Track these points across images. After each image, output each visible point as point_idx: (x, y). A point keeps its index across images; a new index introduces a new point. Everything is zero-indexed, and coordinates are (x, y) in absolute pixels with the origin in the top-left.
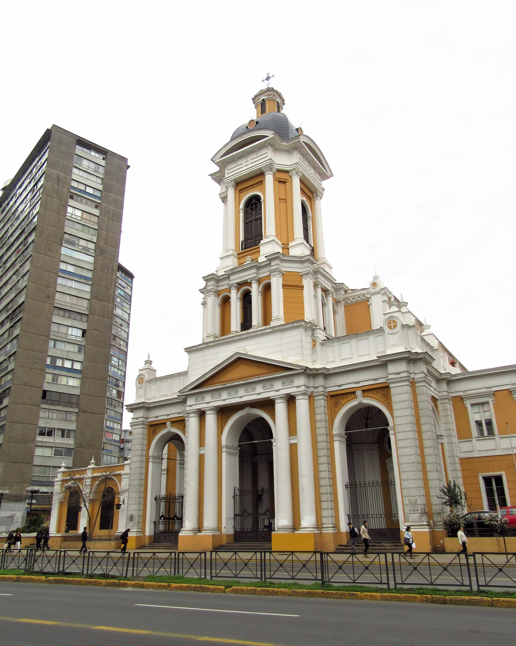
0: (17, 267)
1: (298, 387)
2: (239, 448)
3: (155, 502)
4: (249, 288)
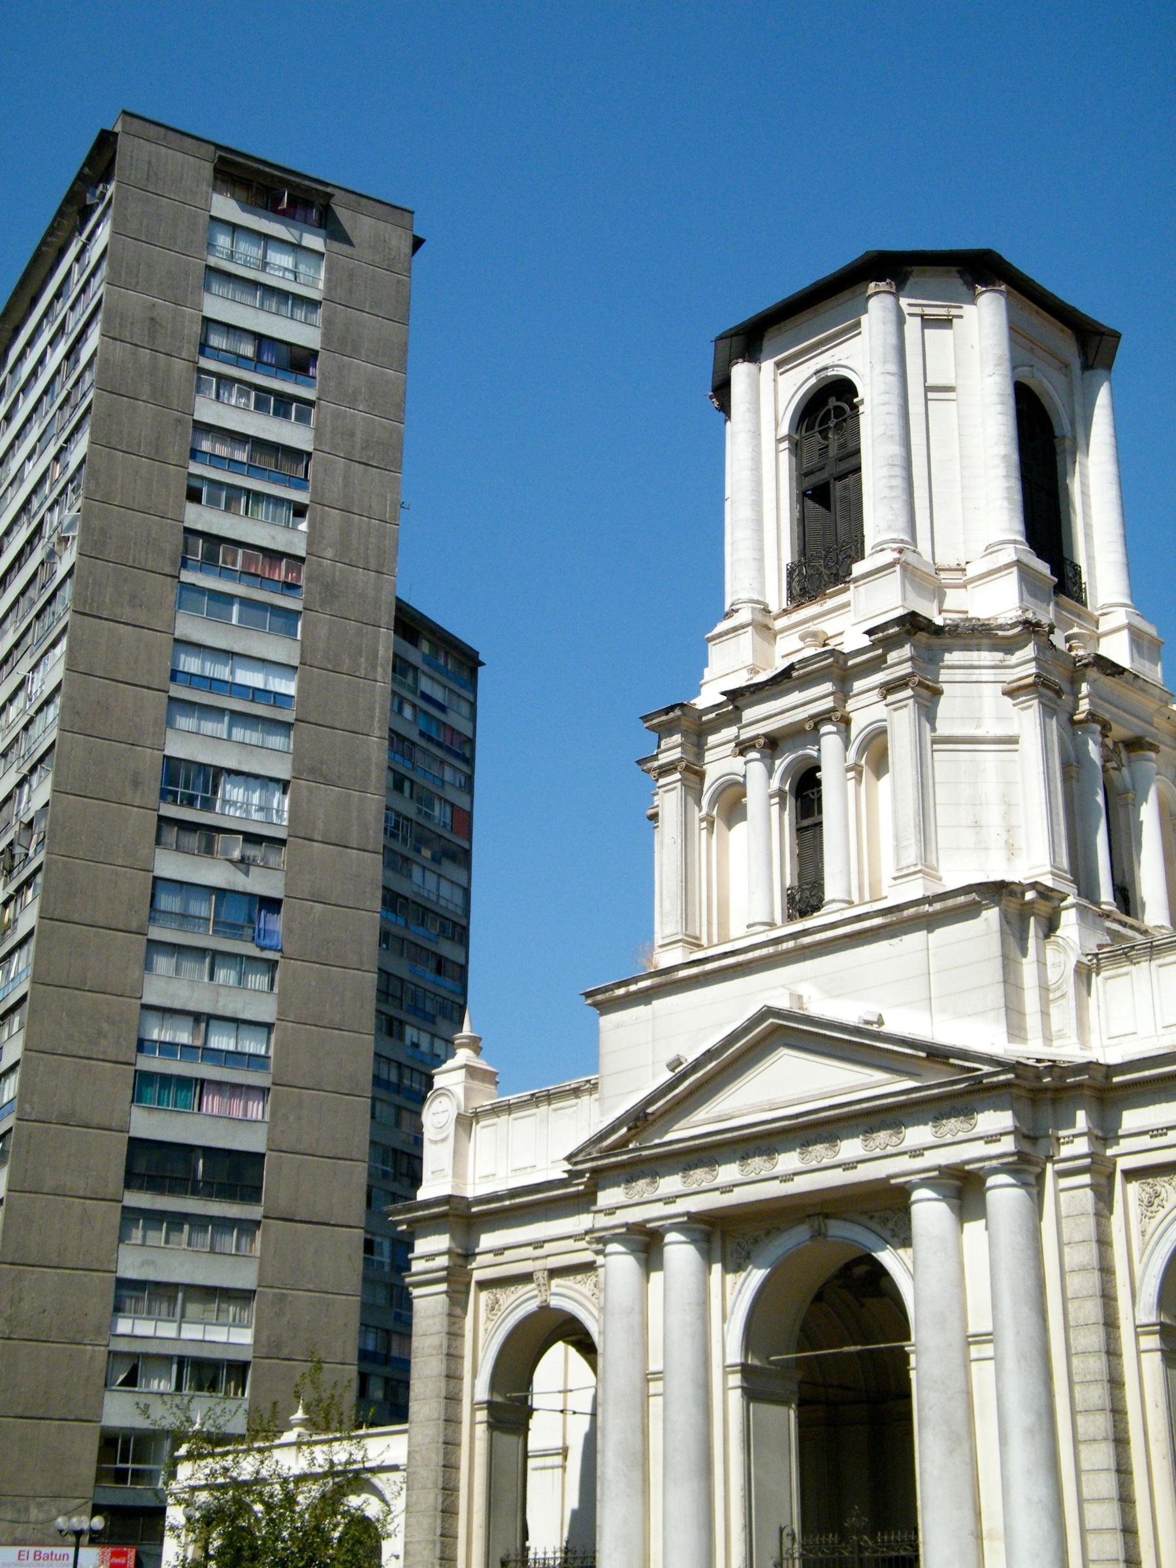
0: (23, 668)
4: (811, 751)
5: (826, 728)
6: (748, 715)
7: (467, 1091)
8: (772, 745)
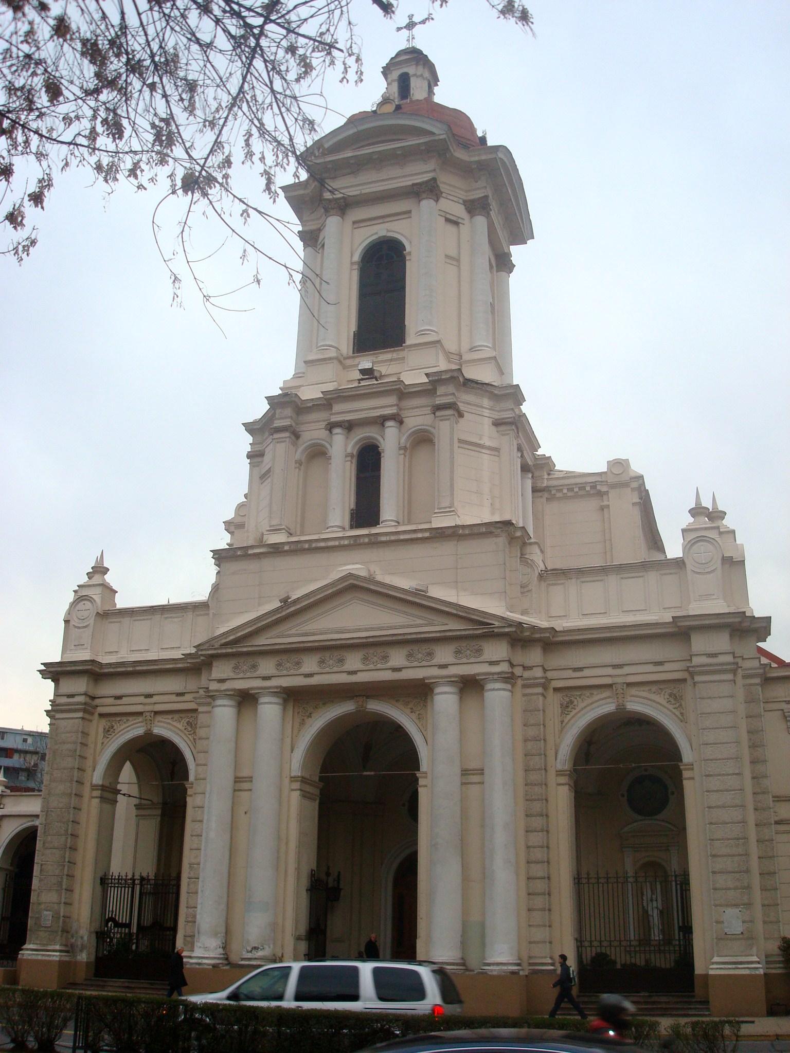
1: (492, 663)
2: (321, 785)
5: (389, 423)
6: (337, 408)
7: (103, 599)
8: (349, 427)
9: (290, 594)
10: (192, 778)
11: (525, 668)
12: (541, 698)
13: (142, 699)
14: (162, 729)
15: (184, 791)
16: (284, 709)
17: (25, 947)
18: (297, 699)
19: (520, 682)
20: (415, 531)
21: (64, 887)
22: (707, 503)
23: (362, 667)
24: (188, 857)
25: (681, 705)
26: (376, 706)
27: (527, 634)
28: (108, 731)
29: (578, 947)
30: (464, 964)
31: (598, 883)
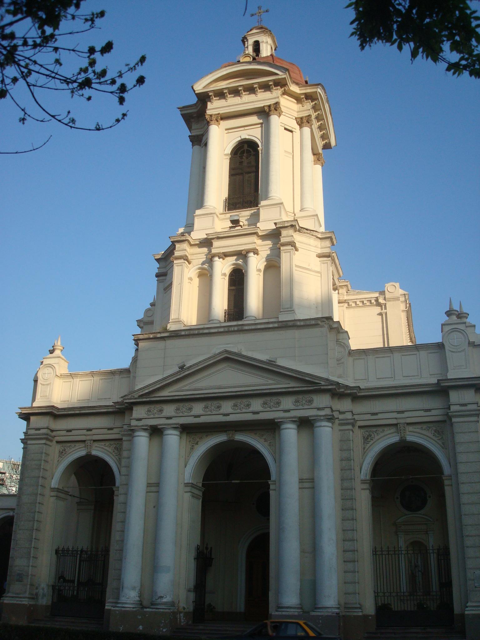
2: (203, 489)
3: (54, 556)
9: (185, 363)
10: (117, 484)
11: (341, 413)
12: (351, 432)
13: (85, 432)
14: (97, 451)
15: (113, 492)
16: (181, 438)
17: (4, 595)
18: (189, 430)
19: (337, 422)
20: (268, 323)
21: (32, 556)
22: (456, 307)
23: (232, 411)
24: (115, 536)
25: (442, 438)
26: (240, 437)
27: (342, 390)
28: (62, 453)
29: (375, 596)
30: (301, 608)
31: (382, 554)
